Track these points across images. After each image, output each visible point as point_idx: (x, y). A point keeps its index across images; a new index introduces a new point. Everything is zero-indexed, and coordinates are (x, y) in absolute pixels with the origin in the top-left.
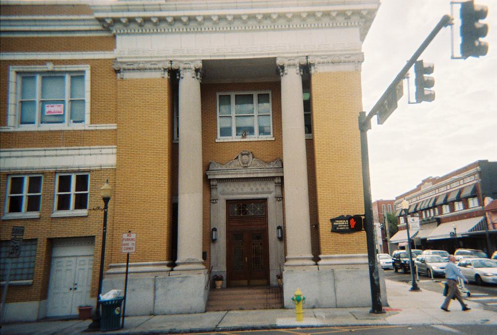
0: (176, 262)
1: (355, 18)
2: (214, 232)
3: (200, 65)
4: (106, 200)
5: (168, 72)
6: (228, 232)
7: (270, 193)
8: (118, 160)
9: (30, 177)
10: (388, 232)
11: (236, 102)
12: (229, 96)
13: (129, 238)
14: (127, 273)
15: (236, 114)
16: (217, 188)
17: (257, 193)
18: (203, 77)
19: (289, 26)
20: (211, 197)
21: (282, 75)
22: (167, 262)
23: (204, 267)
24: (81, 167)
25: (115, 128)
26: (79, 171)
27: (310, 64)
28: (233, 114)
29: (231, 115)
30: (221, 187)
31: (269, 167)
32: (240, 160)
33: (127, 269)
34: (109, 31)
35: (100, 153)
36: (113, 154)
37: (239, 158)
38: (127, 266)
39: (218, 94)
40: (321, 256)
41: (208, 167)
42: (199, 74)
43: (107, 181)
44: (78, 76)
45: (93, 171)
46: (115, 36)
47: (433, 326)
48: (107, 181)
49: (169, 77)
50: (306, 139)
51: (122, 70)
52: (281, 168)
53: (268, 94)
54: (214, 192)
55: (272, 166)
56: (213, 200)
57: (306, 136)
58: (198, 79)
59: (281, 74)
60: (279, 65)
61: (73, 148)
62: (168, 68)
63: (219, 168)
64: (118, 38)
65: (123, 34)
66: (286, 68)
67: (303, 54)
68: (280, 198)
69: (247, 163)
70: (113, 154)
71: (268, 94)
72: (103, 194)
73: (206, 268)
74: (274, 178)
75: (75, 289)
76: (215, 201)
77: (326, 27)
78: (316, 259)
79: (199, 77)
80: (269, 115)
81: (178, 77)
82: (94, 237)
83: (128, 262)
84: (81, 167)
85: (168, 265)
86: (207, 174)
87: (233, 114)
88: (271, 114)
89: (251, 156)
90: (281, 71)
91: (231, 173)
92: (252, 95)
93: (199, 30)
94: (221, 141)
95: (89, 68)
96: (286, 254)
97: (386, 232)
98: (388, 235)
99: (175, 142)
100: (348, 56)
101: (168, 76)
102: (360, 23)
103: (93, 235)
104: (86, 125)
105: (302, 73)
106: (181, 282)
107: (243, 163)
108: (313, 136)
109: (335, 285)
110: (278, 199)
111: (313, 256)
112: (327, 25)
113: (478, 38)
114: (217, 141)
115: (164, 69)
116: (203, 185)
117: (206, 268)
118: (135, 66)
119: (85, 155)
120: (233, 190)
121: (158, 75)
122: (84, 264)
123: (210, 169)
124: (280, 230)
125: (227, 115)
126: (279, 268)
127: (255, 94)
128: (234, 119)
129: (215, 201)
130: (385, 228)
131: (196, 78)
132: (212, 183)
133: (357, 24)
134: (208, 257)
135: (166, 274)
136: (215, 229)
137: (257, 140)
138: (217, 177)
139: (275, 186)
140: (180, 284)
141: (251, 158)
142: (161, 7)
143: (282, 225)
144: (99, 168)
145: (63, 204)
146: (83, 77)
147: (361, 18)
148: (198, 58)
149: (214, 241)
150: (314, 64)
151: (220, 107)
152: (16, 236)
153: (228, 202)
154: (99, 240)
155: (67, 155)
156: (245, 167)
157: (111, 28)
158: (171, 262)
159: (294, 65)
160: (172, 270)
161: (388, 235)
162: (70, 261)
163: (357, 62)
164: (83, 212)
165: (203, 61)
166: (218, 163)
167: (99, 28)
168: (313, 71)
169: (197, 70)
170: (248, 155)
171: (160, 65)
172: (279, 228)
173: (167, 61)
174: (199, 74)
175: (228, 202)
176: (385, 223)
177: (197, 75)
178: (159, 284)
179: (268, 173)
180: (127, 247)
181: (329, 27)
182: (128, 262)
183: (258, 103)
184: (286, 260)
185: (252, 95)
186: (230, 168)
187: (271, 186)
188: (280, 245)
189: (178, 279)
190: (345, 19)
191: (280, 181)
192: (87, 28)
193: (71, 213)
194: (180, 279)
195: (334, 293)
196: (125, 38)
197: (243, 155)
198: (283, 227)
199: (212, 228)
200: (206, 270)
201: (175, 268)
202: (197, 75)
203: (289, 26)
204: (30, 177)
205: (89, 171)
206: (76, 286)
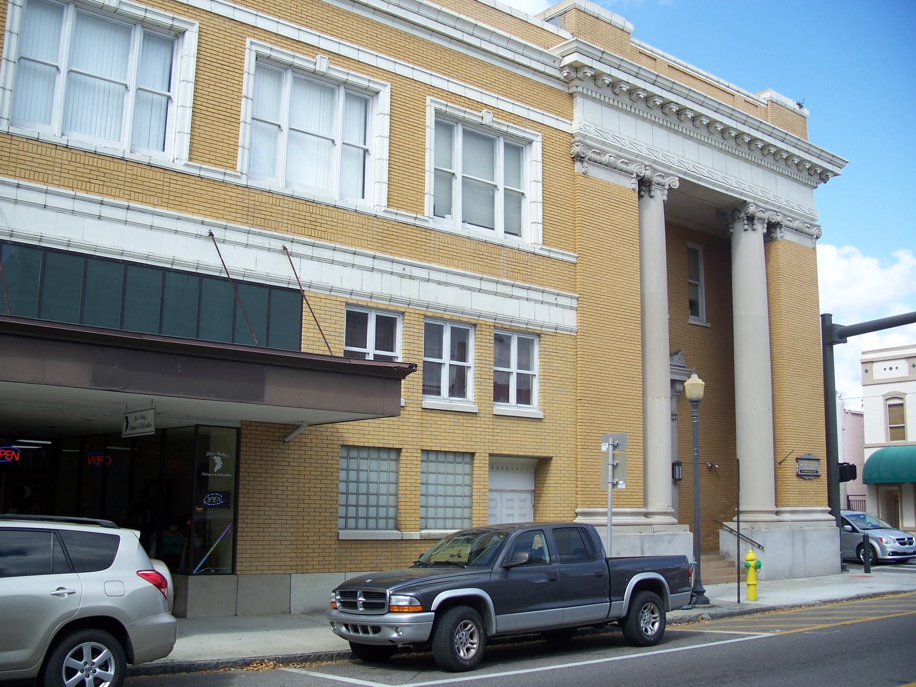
2: (677, 467)
3: (676, 185)
24: (532, 325)
25: (574, 260)
35: (402, 272)
44: (516, 148)
45: (545, 334)
46: (571, 95)
47: (494, 639)
51: (586, 159)
61: (158, 209)
64: (579, 100)
70: (571, 308)
84: (532, 325)
100: (598, 151)
104: (453, 224)
109: (804, 546)
144: (554, 331)
145: (501, 393)
152: (262, 456)
155: (333, 262)
159: (764, 220)
163: (815, 236)
164: (457, 403)
171: (632, 168)
192: (540, 67)
196: (589, 104)
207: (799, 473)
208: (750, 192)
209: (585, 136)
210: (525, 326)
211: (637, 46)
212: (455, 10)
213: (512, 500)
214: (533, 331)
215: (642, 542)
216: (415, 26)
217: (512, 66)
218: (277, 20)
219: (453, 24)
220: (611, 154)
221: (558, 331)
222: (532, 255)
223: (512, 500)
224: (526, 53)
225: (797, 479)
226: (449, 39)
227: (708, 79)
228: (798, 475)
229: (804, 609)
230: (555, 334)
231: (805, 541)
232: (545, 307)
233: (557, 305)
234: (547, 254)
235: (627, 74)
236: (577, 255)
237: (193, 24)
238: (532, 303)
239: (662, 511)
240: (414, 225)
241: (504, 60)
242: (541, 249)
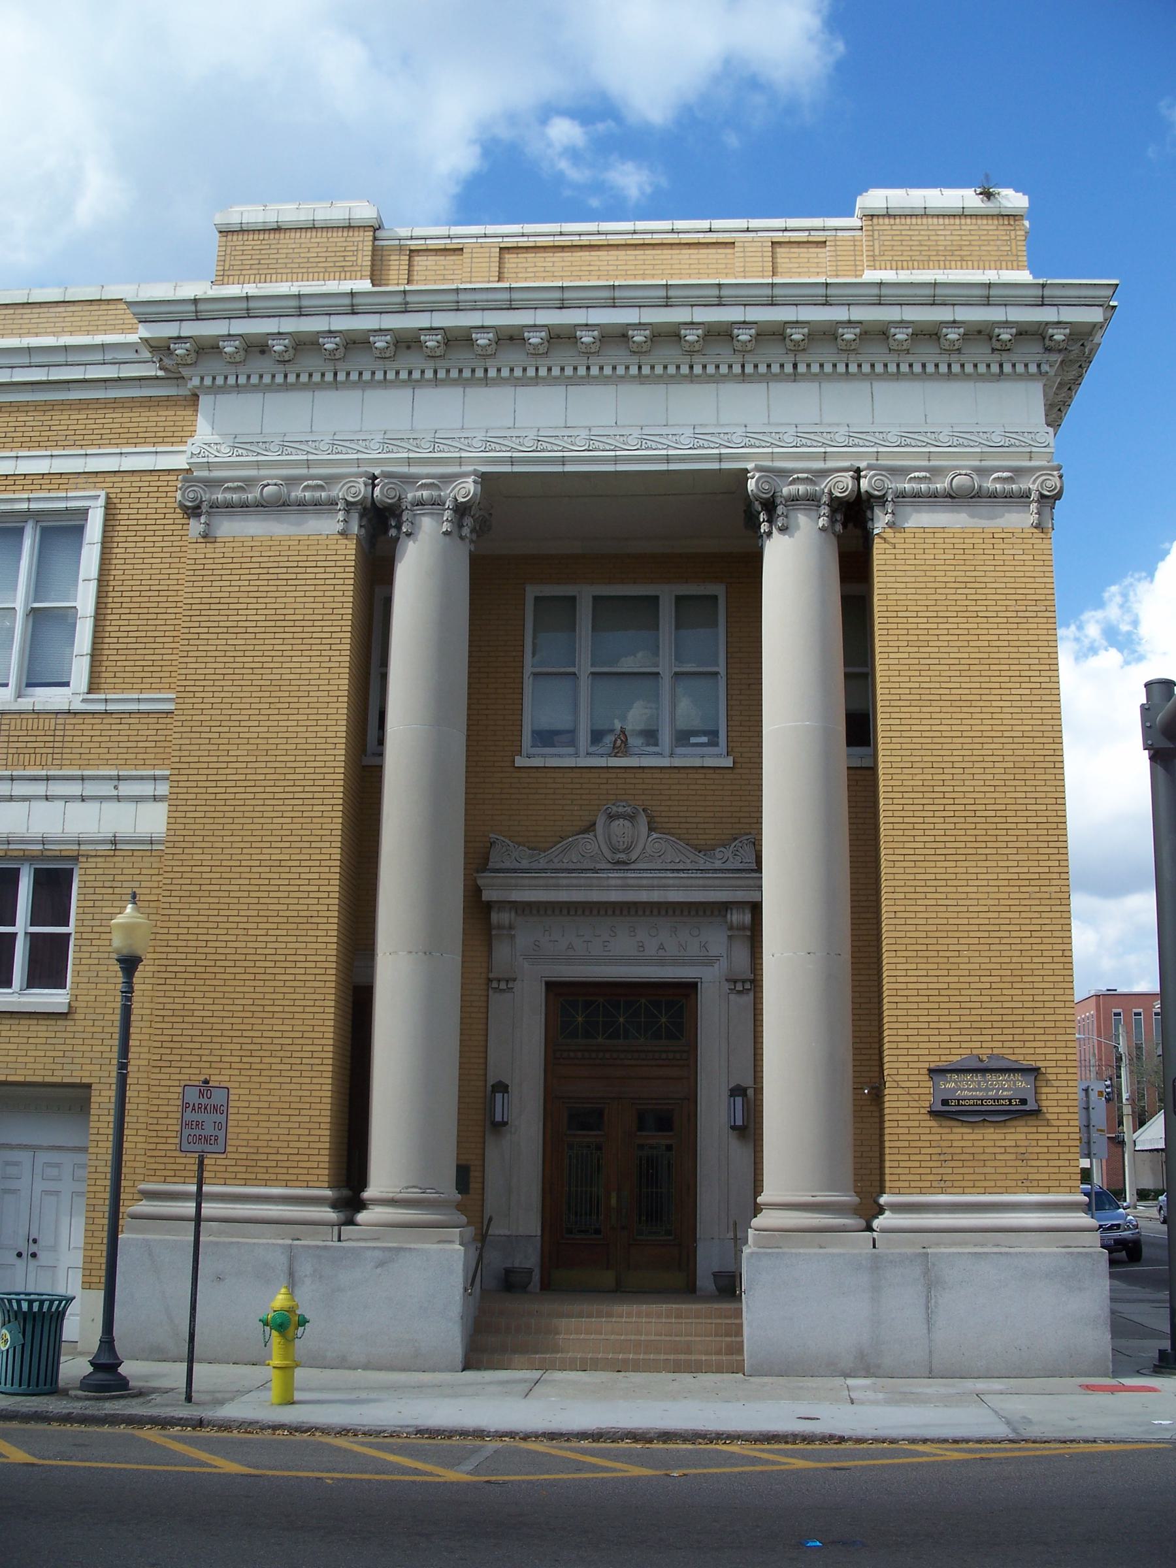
0: (366, 1195)
1: (1031, 352)
2: (499, 1096)
4: (129, 964)
5: (362, 516)
6: (551, 1098)
7: (709, 962)
8: (172, 820)
9: (36, 869)
10: (1127, 1110)
11: (593, 627)
12: (573, 599)
13: (204, 1101)
14: (198, 1219)
15: (592, 665)
16: (513, 937)
17: (662, 962)
18: (482, 528)
19: (795, 366)
20: (489, 970)
21: (769, 534)
22: (328, 1193)
23: (464, 1219)
26: (42, 857)
27: (870, 495)
28: (584, 667)
29: (574, 670)
30: (527, 935)
31: (708, 866)
32: (600, 838)
33: (199, 1208)
34: (180, 379)
35: (115, 793)
36: (155, 798)
37: (599, 828)
38: (199, 1197)
39: (532, 592)
40: (884, 1199)
41: (486, 859)
42: (468, 521)
43: (134, 895)
45: (88, 856)
46: (195, 397)
48: (134, 895)
49: (363, 531)
50: (848, 768)
51: (204, 508)
52: (753, 870)
53: (715, 598)
54: (502, 952)
55: (718, 864)
56: (499, 981)
57: (849, 756)
58: (462, 538)
59: (764, 527)
60: (757, 498)
62: (362, 502)
63: (525, 864)
65: (223, 389)
66: (780, 510)
67: (846, 464)
68: (744, 982)
69: (628, 850)
71: (715, 598)
72: (118, 941)
73: (469, 1224)
74: (724, 907)
75: (34, 1255)
76: (503, 986)
77: (924, 375)
78: (869, 1210)
79: (466, 531)
80: (717, 673)
81: (393, 532)
82: (89, 1086)
83: (200, 1185)
85: (335, 1205)
86: (479, 882)
87: (584, 667)
88: (721, 669)
89: (643, 821)
90: (762, 517)
91: (565, 882)
92: (657, 598)
93: (480, 373)
94: (537, 762)
95: (101, 502)
96: (758, 1188)
97: (1120, 1109)
98: (1128, 1122)
99: (370, 761)
101: (361, 526)
102: (1045, 368)
103: (85, 1081)
105: (839, 528)
106: (381, 1264)
107: (614, 850)
108: (875, 756)
109: (928, 1299)
110: (739, 987)
111: (857, 1200)
112: (930, 369)
113: (1081, 612)
114: (520, 762)
115: (348, 503)
116: (464, 933)
117: (469, 1224)
118: (251, 496)
119: (67, 799)
120: (570, 947)
121: (330, 525)
122: (58, 1179)
123: (491, 865)
124: (739, 1100)
125: (562, 670)
126: (731, 1235)
127: (667, 594)
128: (584, 683)
129: (503, 986)
130: (1120, 1095)
131: (455, 534)
132: (495, 917)
133: (1033, 369)
134: (474, 1185)
135: (324, 1239)
136: (501, 1088)
137: (665, 762)
138: (516, 896)
139: (730, 937)
140: (379, 1270)
141: (644, 829)
142: (356, 301)
143: (748, 1082)
144: (109, 847)
146: (78, 531)
147: (1048, 350)
148: (466, 469)
149: (498, 1127)
150: (882, 500)
151: (534, 638)
153: (554, 988)
154: (103, 1099)
156: (618, 862)
157: (185, 372)
158: (346, 1192)
160: (351, 1222)
161: (1128, 1122)
162: (16, 1164)
164: (53, 999)
165: (485, 479)
166: (519, 844)
167: (152, 371)
168: (880, 521)
169: (461, 510)
170: (631, 818)
171: (338, 492)
172: (738, 1091)
173: (360, 475)
174: (468, 521)
175: (554, 988)
176: (1119, 1077)
177: (461, 526)
178: (305, 1268)
179: (705, 888)
180: (197, 1132)
181: (937, 376)
182: (200, 1185)
183: (677, 627)
184: (757, 1210)
185: (657, 598)
186: (564, 866)
187: (715, 940)
188: (739, 1151)
189: (369, 1253)
190: (993, 350)
191: (747, 918)
193: (15, 998)
194: (377, 1253)
195: (925, 1326)
197: (612, 817)
198: (750, 1092)
199: (491, 1082)
200: (470, 1231)
201: (361, 1217)
202: (461, 526)
203: (795, 366)
204: (36, 869)
205: (75, 859)
206: (33, 1248)
207: (939, 1107)
208: (751, 446)
209: (209, 466)
210: (40, 847)
211: (480, 240)
212: (47, 334)
213: (58, 1165)
214: (58, 853)
215: (291, 1260)
216: (143, 382)
217: (49, 390)
218: (118, 451)
219: (26, 361)
220: (265, 482)
221: (119, 847)
222: (65, 716)
223: (58, 1165)
224: (71, 359)
225: (933, 1123)
226: (138, 382)
227: (635, 236)
228: (934, 1114)
229: (282, 1435)
230: (112, 853)
231: (931, 1283)
232: (92, 807)
233: (118, 798)
234: (101, 707)
235: (277, 319)
236: (174, 696)
237: (97, 497)
238: (60, 804)
239: (385, 1195)
240: (106, 712)
241: (35, 387)
242: (84, 701)
